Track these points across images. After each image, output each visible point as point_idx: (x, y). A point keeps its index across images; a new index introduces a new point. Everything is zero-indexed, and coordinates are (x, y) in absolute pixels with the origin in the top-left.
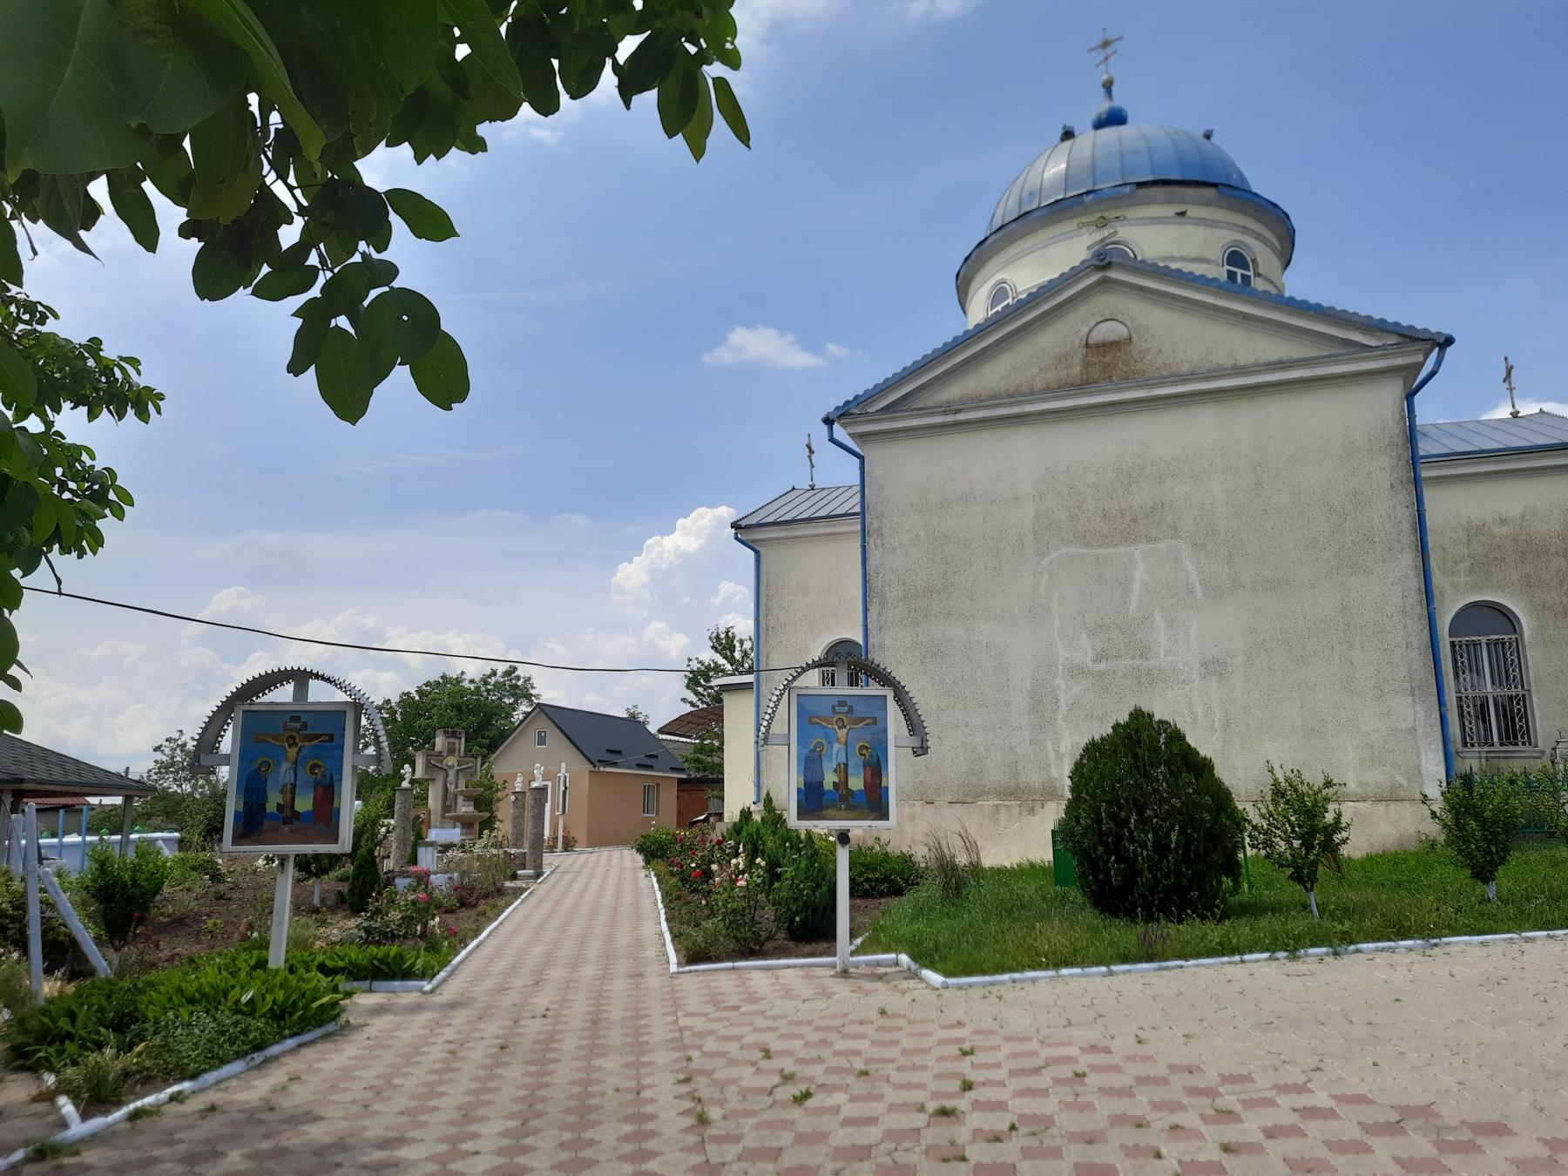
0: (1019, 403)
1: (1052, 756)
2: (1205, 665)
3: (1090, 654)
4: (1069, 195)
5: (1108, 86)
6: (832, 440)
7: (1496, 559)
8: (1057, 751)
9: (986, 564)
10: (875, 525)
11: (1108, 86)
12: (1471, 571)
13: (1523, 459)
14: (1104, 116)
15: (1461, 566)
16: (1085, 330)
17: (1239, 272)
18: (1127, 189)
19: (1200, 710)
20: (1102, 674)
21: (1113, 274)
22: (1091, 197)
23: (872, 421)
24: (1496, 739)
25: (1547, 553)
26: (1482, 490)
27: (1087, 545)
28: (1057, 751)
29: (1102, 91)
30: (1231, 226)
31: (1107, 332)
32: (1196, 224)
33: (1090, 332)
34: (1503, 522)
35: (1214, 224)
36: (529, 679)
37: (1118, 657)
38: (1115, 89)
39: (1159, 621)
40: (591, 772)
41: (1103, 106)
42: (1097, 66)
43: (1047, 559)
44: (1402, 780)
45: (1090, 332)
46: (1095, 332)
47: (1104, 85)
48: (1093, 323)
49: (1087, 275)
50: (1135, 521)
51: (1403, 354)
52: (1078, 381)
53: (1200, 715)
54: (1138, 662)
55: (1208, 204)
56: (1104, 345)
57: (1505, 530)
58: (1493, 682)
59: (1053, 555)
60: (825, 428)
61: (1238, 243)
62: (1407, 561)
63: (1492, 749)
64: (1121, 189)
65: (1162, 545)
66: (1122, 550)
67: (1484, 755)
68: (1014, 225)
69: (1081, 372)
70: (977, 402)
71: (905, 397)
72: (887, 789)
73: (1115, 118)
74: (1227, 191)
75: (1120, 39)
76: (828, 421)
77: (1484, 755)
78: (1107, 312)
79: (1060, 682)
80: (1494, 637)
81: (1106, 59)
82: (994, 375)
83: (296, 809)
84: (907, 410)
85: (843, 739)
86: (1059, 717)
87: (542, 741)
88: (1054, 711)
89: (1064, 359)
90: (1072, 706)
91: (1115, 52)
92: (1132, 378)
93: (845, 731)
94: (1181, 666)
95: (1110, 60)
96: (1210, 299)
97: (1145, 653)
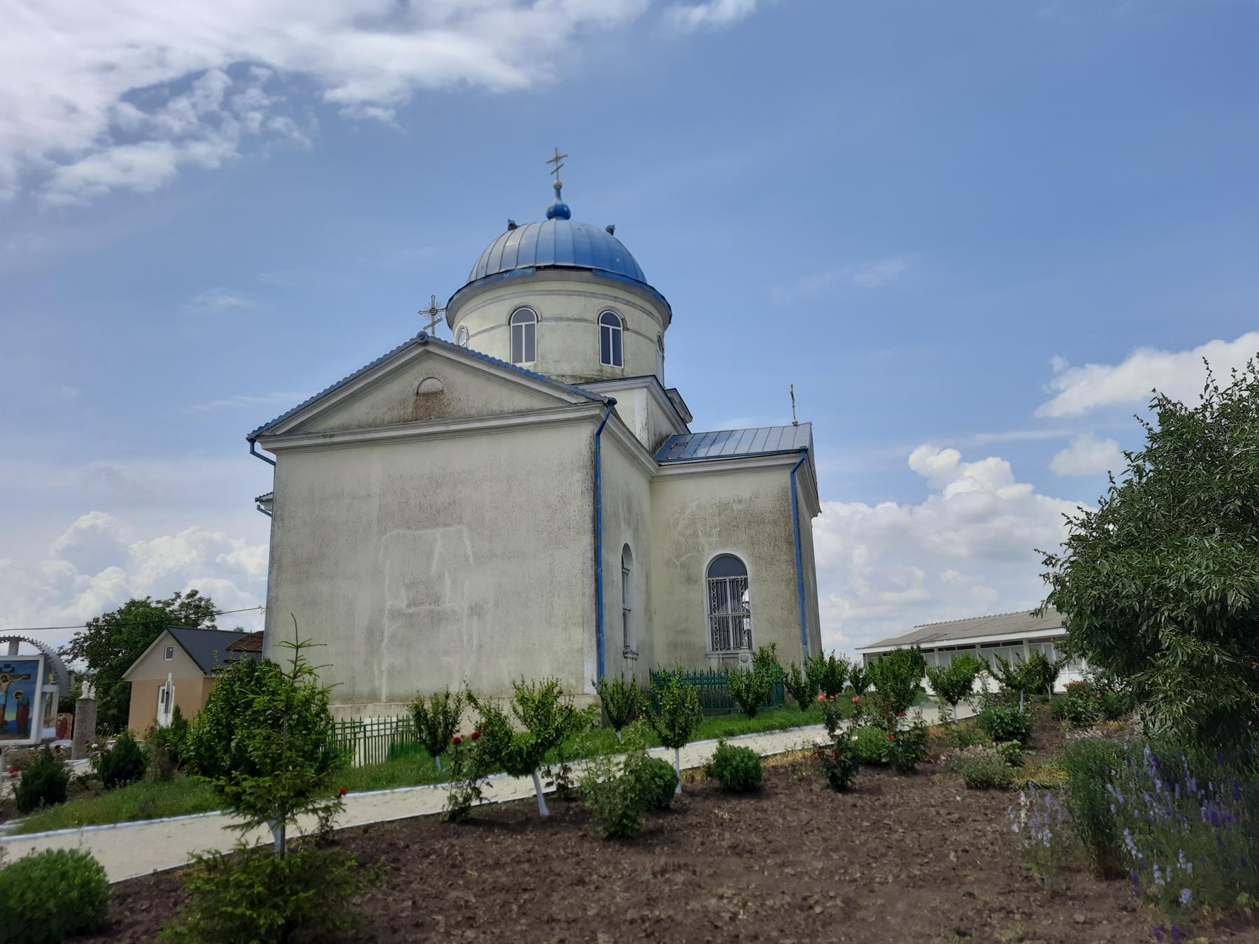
0: (369, 432)
1: (376, 672)
2: (471, 608)
3: (406, 601)
4: (519, 267)
5: (558, 188)
6: (253, 452)
7: (734, 526)
8: (379, 669)
9: (347, 540)
10: (279, 513)
11: (558, 188)
12: (720, 534)
13: (711, 465)
14: (551, 210)
15: (714, 531)
16: (417, 384)
17: (611, 327)
18: (530, 271)
19: (465, 638)
20: (411, 615)
21: (430, 348)
22: (508, 274)
23: (277, 441)
24: (728, 584)
25: (763, 522)
26: (729, 480)
27: (409, 528)
28: (379, 669)
29: (554, 190)
30: (606, 297)
31: (429, 386)
32: (579, 295)
33: (420, 385)
34: (740, 502)
35: (593, 295)
36: (209, 600)
37: (422, 604)
38: (562, 191)
39: (448, 581)
40: (204, 678)
41: (553, 202)
42: (552, 173)
43: (384, 538)
44: (573, 681)
45: (420, 385)
46: (423, 385)
47: (555, 187)
48: (421, 379)
49: (415, 348)
50: (438, 512)
51: (589, 409)
52: (411, 418)
53: (465, 642)
54: (433, 607)
55: (588, 282)
56: (428, 394)
57: (740, 507)
58: (727, 618)
59: (388, 535)
60: (249, 444)
61: (611, 308)
62: (587, 540)
63: (728, 652)
64: (526, 270)
65: (453, 529)
66: (430, 531)
67: (721, 656)
68: (465, 290)
69: (413, 411)
70: (345, 429)
71: (303, 424)
72: (31, 719)
73: (560, 213)
74: (599, 273)
75: (566, 156)
76: (252, 441)
77: (721, 656)
78: (430, 372)
79: (386, 621)
80: (732, 577)
81: (557, 169)
82: (360, 411)
83: (5, 719)
84: (305, 434)
85: (5, 689)
86: (383, 645)
87: (170, 655)
88: (381, 641)
89: (403, 402)
90: (392, 637)
91: (562, 165)
92: (442, 418)
93: (7, 683)
94: (457, 609)
95: (560, 170)
96: (485, 368)
97: (437, 601)
